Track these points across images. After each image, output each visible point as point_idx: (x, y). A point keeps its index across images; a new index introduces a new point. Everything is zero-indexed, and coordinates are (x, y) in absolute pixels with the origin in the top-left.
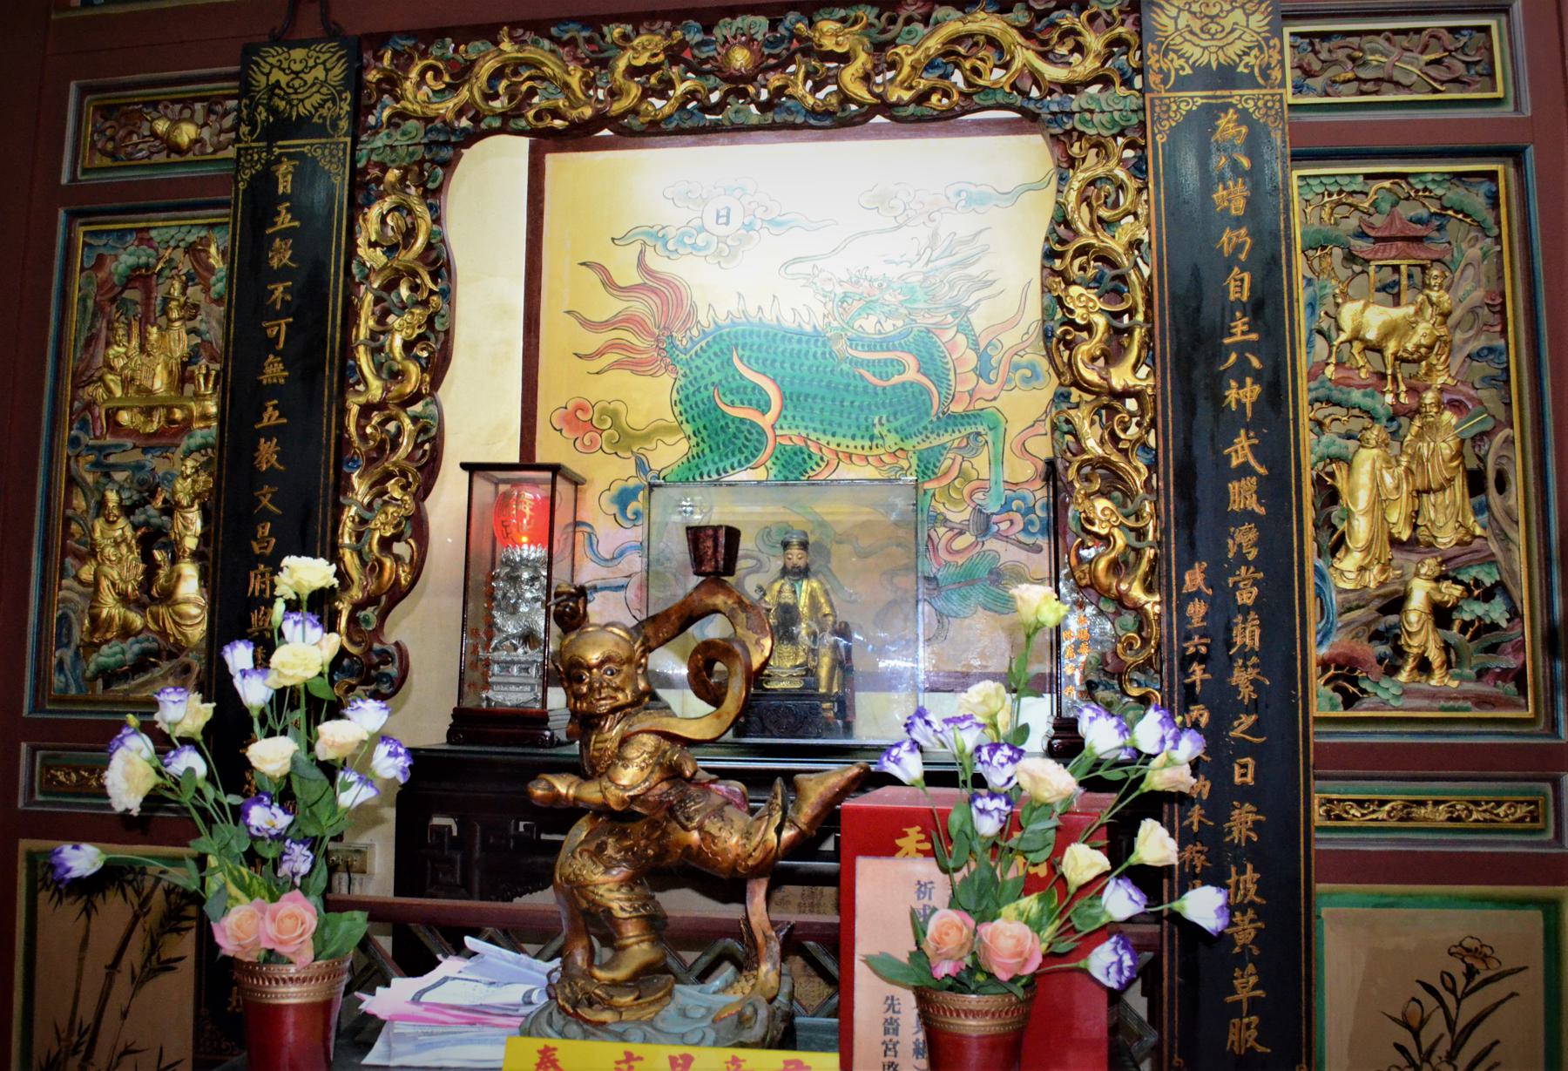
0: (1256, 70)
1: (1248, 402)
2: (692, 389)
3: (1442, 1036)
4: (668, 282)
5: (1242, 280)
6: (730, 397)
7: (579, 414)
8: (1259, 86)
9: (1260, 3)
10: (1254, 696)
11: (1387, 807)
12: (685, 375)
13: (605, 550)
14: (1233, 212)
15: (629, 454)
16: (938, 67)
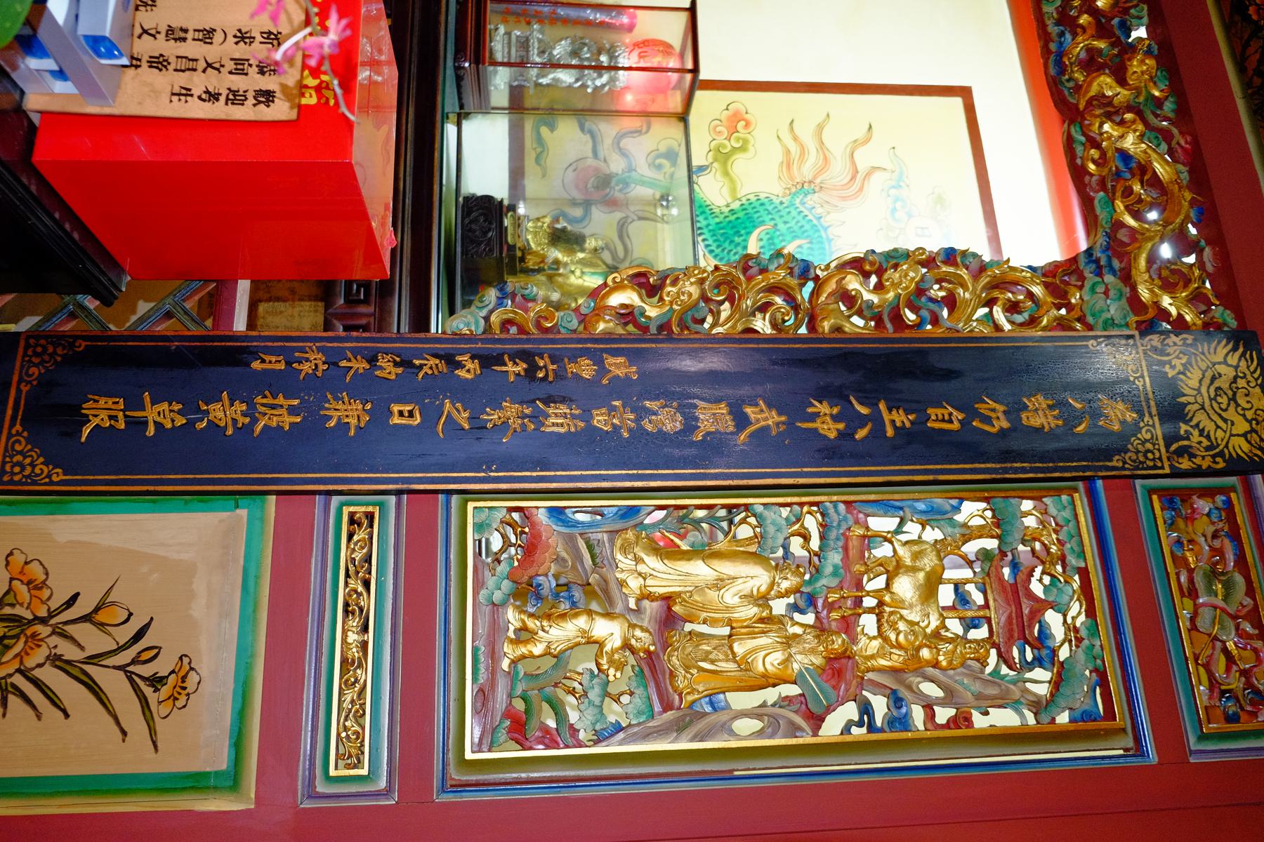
0: (1186, 443)
1: (817, 425)
2: (770, 208)
3: (82, 648)
4: (861, 189)
5: (951, 421)
6: (765, 238)
7: (742, 123)
8: (1167, 446)
9: (1260, 448)
10: (489, 425)
11: (360, 589)
12: (782, 203)
13: (627, 143)
14: (1024, 416)
15: (711, 160)
16: (1126, 165)
